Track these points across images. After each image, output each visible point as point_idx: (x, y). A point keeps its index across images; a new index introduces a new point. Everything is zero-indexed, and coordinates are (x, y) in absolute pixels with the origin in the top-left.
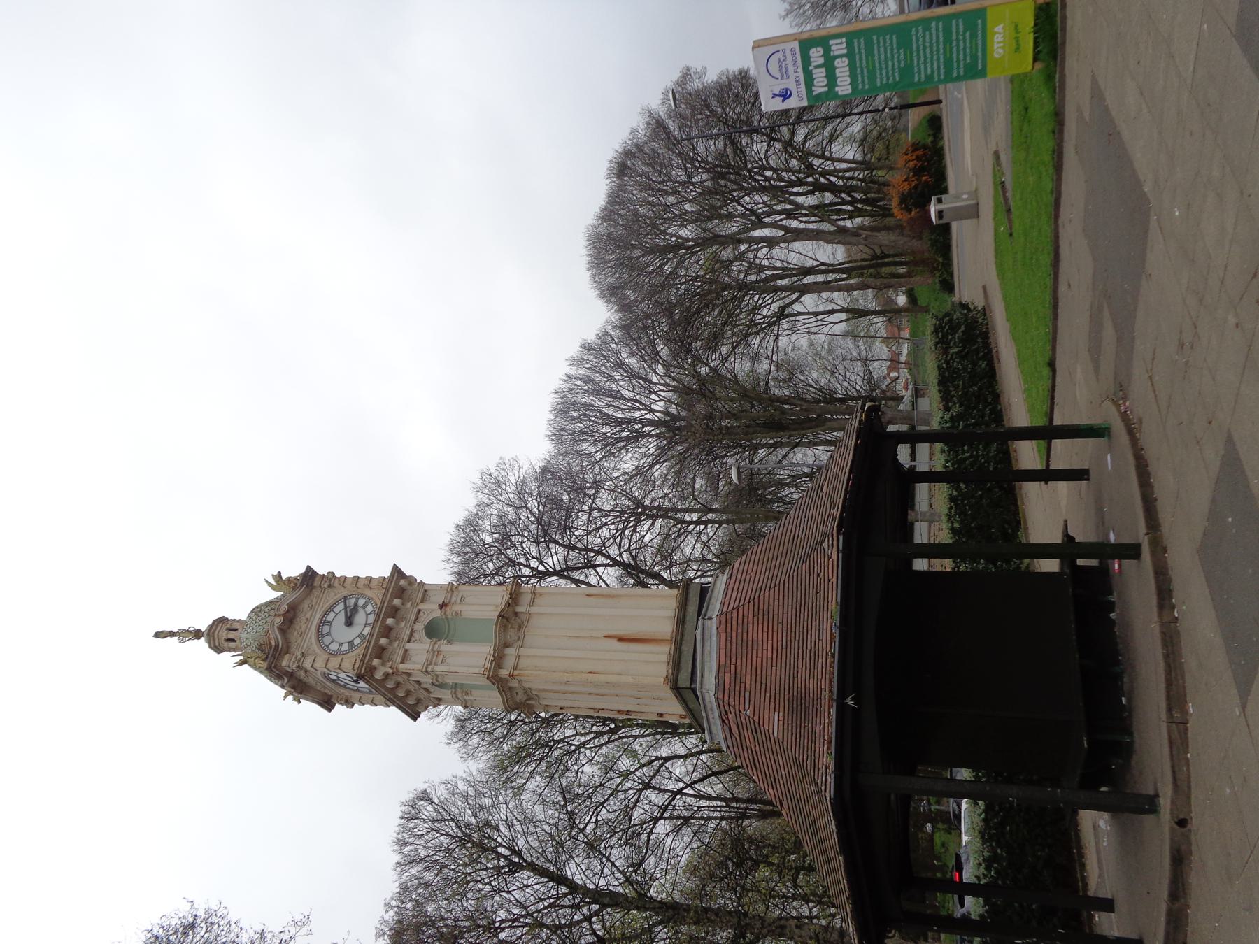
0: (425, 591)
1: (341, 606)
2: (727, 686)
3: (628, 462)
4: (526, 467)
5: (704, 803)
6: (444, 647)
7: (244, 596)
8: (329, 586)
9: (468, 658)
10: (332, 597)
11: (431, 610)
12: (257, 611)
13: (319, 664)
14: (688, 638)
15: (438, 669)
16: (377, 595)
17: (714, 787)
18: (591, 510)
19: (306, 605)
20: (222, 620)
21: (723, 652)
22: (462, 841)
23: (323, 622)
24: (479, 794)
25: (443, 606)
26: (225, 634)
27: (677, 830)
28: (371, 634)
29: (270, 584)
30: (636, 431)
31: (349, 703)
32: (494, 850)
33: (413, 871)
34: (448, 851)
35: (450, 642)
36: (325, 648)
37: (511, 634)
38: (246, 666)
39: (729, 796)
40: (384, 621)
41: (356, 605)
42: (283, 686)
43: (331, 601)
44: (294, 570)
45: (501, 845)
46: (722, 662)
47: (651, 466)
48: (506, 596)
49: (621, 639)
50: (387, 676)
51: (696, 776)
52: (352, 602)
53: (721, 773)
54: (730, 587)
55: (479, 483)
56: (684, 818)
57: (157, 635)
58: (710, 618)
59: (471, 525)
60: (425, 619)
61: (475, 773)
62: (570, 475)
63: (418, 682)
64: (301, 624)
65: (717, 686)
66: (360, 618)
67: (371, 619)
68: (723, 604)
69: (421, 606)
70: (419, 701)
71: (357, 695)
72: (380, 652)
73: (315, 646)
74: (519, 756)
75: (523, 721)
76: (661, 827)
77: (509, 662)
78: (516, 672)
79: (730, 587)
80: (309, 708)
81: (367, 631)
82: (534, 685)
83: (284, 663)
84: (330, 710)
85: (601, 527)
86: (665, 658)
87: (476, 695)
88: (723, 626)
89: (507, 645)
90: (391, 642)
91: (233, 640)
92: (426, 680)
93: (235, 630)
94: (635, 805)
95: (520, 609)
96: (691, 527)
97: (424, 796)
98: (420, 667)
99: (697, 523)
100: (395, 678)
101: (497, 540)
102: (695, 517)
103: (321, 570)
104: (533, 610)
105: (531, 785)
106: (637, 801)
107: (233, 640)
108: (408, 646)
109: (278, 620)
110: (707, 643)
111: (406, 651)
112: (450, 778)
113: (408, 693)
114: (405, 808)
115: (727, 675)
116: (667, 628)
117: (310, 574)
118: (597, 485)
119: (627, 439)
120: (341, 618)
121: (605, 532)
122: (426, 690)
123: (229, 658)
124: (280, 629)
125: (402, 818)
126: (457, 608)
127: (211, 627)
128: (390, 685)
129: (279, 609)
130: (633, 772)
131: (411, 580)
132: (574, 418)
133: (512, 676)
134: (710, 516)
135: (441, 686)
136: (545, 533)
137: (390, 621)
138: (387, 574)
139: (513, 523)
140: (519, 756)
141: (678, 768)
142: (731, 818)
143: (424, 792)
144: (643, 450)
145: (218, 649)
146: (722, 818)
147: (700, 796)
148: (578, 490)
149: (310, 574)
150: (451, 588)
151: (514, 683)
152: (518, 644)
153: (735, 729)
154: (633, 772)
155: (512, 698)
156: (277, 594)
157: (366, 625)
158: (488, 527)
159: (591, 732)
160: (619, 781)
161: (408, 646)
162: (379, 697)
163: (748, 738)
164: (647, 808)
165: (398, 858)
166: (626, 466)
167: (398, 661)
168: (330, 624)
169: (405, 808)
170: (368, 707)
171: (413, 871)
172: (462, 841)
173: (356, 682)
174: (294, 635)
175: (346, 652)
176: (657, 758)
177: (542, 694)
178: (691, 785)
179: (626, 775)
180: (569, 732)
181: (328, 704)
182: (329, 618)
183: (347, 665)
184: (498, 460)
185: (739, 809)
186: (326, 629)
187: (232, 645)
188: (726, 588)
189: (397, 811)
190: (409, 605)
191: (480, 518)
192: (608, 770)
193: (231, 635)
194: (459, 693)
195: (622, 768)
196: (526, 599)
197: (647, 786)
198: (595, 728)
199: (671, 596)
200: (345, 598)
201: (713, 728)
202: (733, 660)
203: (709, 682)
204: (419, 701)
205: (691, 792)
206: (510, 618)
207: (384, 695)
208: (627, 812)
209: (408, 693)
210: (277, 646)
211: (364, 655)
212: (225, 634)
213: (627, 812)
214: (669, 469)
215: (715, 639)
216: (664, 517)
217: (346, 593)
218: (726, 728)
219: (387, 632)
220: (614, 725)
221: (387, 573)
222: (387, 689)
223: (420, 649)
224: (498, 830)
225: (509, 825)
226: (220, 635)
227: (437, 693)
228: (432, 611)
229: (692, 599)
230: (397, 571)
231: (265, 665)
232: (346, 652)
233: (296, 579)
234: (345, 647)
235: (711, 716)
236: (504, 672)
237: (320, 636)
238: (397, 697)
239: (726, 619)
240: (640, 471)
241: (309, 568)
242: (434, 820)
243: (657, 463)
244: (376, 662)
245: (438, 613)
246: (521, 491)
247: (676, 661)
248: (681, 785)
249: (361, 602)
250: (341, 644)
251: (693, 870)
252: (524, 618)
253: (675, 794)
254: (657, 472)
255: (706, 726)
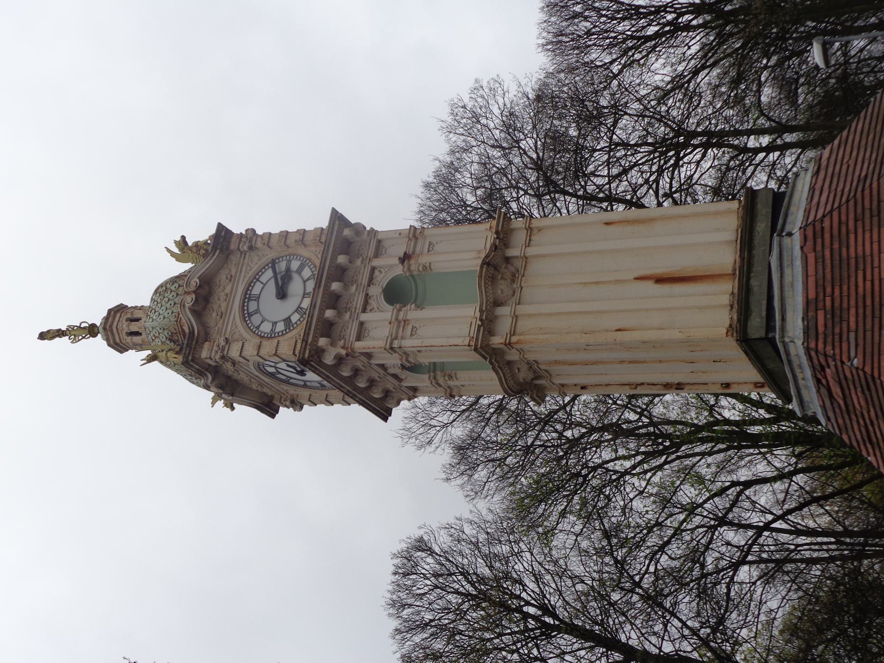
0: (377, 241)
1: (269, 273)
2: (821, 329)
3: (660, 70)
4: (513, 92)
5: (802, 540)
6: (412, 313)
7: (143, 273)
8: (251, 248)
9: (446, 327)
10: (254, 263)
11: (389, 267)
12: (162, 291)
13: (250, 351)
14: (758, 268)
15: (408, 343)
16: (314, 254)
17: (818, 518)
18: (613, 146)
19: (223, 276)
20: (120, 309)
21: (811, 280)
22: (478, 599)
23: (247, 297)
24: (492, 540)
25: (405, 258)
26: (125, 327)
27: (767, 578)
28: (313, 305)
29: (173, 254)
30: (669, 23)
31: (296, 405)
32: (519, 610)
33: (417, 639)
34: (460, 613)
35: (419, 307)
36: (255, 331)
37: (503, 287)
38: (156, 363)
39: (840, 528)
40: (327, 286)
41: (288, 270)
42: (207, 387)
43: (255, 268)
44: (201, 232)
45: (528, 603)
46: (812, 295)
47: (696, 72)
48: (491, 237)
49: (660, 280)
50: (340, 360)
51: (790, 505)
52: (282, 266)
53: (825, 498)
54: (818, 186)
55: (449, 119)
56: (776, 561)
57: (43, 336)
58: (790, 234)
59: (446, 179)
60: (383, 279)
61: (484, 512)
62: (578, 99)
63: (382, 366)
64: (219, 302)
65: (806, 331)
66: (296, 287)
67: (310, 285)
68: (807, 212)
69: (376, 263)
70: (387, 393)
71: (306, 393)
72: (327, 329)
73: (241, 329)
74: (543, 493)
75: (538, 427)
76: (744, 573)
77: (504, 326)
78: (514, 339)
79: (818, 186)
80: (246, 414)
81: (306, 303)
82: (542, 356)
83: (204, 354)
84: (273, 416)
85: (631, 167)
86: (726, 299)
87: (464, 377)
88: (810, 244)
89: (497, 303)
90: (340, 314)
91: (137, 334)
92: (393, 361)
93: (137, 320)
94: (707, 547)
95: (512, 252)
96: (761, 155)
97: (421, 545)
98: (381, 343)
99: (769, 149)
100: (351, 362)
101: (484, 201)
102: (765, 140)
103: (237, 228)
104: (530, 251)
105: (565, 525)
106: (710, 542)
107: (137, 334)
108: (364, 317)
109: (189, 300)
110: (787, 271)
111: (362, 324)
112: (452, 521)
113: (372, 382)
114: (397, 561)
115: (821, 314)
116: (726, 258)
117: (222, 234)
118: (618, 111)
119: (657, 35)
120: (271, 289)
121: (634, 176)
122: (395, 376)
123: (135, 357)
124: (193, 311)
125: (395, 573)
126: (424, 260)
127: (106, 319)
128: (346, 373)
129: (188, 284)
130: (701, 505)
131: (359, 229)
132: (576, 15)
133: (509, 344)
134: (789, 138)
135: (414, 368)
136: (548, 181)
137: (335, 286)
138: (324, 223)
139: (503, 171)
140: (543, 493)
141: (764, 496)
142: (843, 558)
143: (421, 540)
144: (680, 51)
145: (121, 348)
146: (832, 559)
147: (798, 532)
148: (591, 118)
149: (222, 234)
150: (414, 234)
151: (513, 355)
152: (514, 299)
153: (836, 390)
154: (701, 505)
155: (513, 376)
156: (188, 266)
157: (305, 295)
158: (469, 181)
159: (638, 453)
160: (682, 517)
161: (364, 317)
162: (336, 393)
163: (857, 399)
164: (723, 549)
165: (395, 623)
166: (658, 78)
167: (353, 336)
168: (258, 298)
169: (397, 561)
170: (321, 408)
171: (417, 639)
172: (478, 599)
173: (302, 373)
174: (212, 318)
175: (282, 334)
176: (734, 484)
177: (554, 369)
178: (782, 517)
179: (691, 509)
180: (607, 454)
181: (269, 408)
182: (256, 291)
183: (286, 349)
184: (471, 84)
185: (853, 545)
186: (253, 306)
187: (137, 339)
188: (812, 189)
189: (389, 565)
190: (359, 262)
191: (456, 170)
192: (665, 502)
193: (134, 327)
194: (440, 378)
195: (685, 501)
196: (520, 237)
197: (723, 521)
198: (643, 449)
199: (729, 212)
200: (273, 263)
201: (804, 392)
202: (829, 290)
203: (795, 325)
204: (387, 393)
205: (784, 526)
206: (500, 268)
207: (340, 388)
208: (696, 556)
209: (372, 382)
210: (192, 332)
211: (306, 334)
212: (125, 327)
213: (696, 556)
214: (720, 77)
215: (798, 263)
216: (719, 146)
217: (271, 255)
218: (823, 391)
219: (334, 301)
220: (666, 442)
221: (324, 222)
222: (343, 378)
223: (380, 320)
224: (524, 585)
225: (538, 578)
226: (120, 329)
227: (411, 380)
228: (391, 267)
229: (760, 215)
230: (337, 217)
231: (180, 358)
232: (282, 334)
233: (206, 243)
234: (281, 327)
235: (800, 376)
236: (497, 341)
237: (246, 315)
238: (356, 388)
239: (813, 232)
240: (678, 83)
241: (220, 227)
242: (436, 575)
243: (703, 67)
244: (322, 342)
245: (399, 270)
246: (510, 124)
247: (743, 303)
248: (770, 517)
249: (295, 265)
250: (275, 324)
251: (792, 630)
252: (518, 264)
253: (760, 531)
254: (706, 79)
255: (793, 392)
